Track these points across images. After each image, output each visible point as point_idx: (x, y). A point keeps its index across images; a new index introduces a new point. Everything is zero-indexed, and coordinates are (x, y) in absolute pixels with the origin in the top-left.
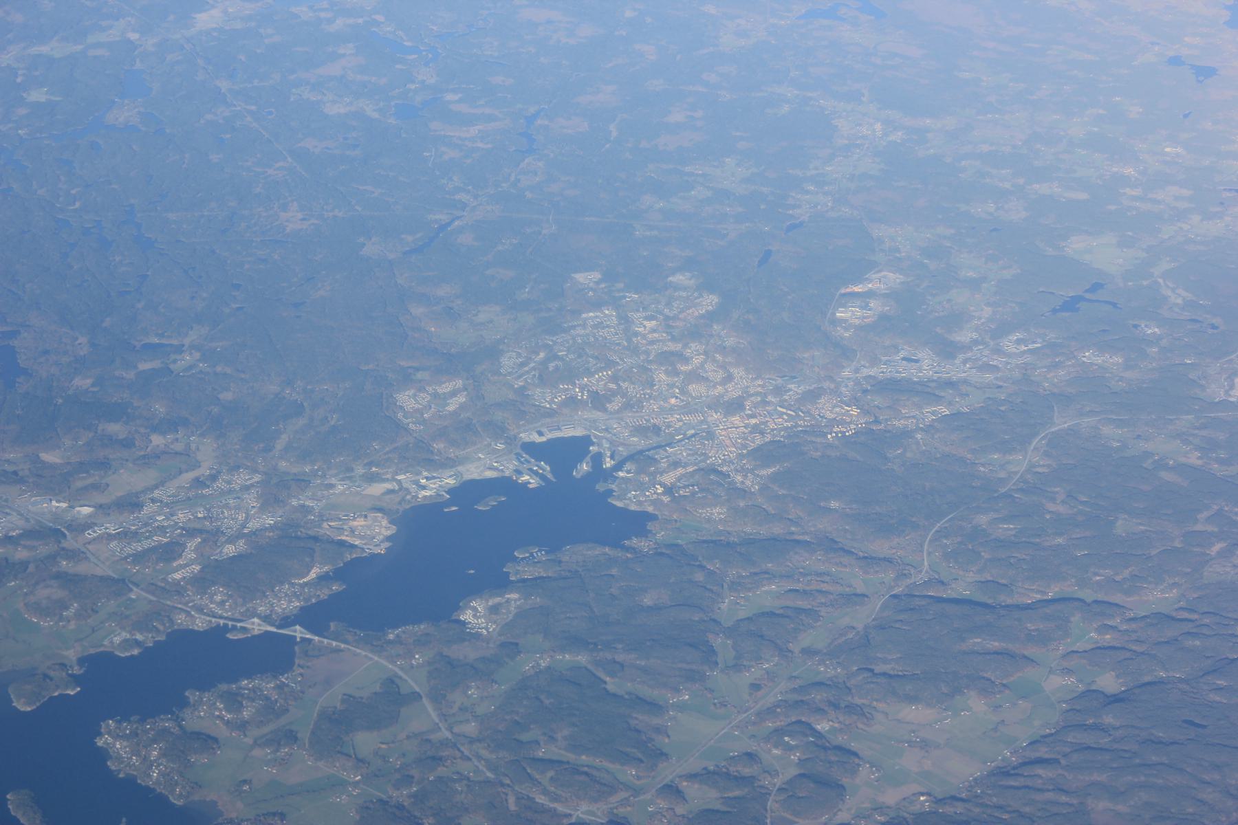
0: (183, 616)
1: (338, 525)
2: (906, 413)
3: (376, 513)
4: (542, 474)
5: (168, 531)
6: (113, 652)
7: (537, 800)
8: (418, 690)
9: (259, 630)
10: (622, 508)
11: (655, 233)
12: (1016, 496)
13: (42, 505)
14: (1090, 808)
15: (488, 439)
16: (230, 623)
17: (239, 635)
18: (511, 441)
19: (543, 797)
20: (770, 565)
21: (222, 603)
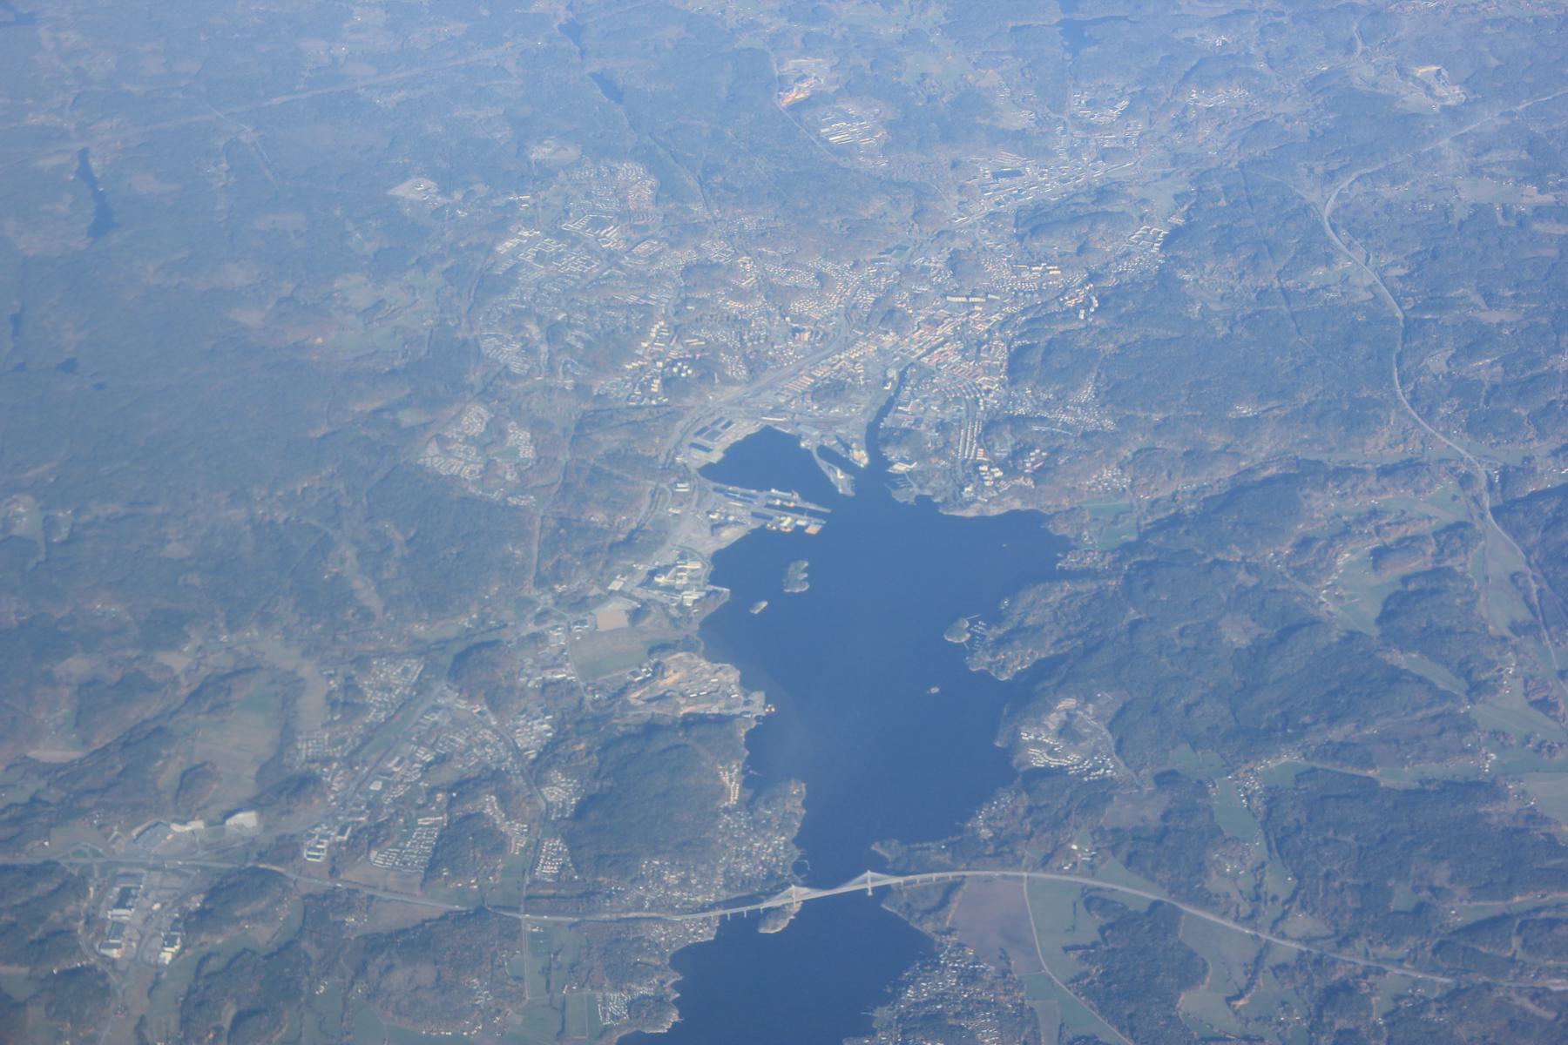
0: (659, 929)
1: (644, 693)
2: (1113, 251)
3: (675, 653)
4: (795, 507)
5: (334, 804)
6: (638, 1032)
7: (1555, 989)
8: (1154, 897)
9: (789, 896)
10: (976, 518)
11: (399, 96)
12: (1427, 317)
13: (165, 838)
14: (370, 286)
15: (650, 482)
16: (745, 909)
17: (779, 923)
18: (684, 474)
19: (1558, 981)
20: (1301, 526)
21: (684, 882)
